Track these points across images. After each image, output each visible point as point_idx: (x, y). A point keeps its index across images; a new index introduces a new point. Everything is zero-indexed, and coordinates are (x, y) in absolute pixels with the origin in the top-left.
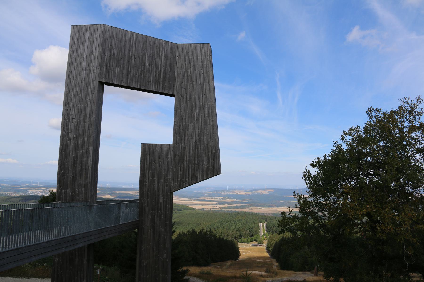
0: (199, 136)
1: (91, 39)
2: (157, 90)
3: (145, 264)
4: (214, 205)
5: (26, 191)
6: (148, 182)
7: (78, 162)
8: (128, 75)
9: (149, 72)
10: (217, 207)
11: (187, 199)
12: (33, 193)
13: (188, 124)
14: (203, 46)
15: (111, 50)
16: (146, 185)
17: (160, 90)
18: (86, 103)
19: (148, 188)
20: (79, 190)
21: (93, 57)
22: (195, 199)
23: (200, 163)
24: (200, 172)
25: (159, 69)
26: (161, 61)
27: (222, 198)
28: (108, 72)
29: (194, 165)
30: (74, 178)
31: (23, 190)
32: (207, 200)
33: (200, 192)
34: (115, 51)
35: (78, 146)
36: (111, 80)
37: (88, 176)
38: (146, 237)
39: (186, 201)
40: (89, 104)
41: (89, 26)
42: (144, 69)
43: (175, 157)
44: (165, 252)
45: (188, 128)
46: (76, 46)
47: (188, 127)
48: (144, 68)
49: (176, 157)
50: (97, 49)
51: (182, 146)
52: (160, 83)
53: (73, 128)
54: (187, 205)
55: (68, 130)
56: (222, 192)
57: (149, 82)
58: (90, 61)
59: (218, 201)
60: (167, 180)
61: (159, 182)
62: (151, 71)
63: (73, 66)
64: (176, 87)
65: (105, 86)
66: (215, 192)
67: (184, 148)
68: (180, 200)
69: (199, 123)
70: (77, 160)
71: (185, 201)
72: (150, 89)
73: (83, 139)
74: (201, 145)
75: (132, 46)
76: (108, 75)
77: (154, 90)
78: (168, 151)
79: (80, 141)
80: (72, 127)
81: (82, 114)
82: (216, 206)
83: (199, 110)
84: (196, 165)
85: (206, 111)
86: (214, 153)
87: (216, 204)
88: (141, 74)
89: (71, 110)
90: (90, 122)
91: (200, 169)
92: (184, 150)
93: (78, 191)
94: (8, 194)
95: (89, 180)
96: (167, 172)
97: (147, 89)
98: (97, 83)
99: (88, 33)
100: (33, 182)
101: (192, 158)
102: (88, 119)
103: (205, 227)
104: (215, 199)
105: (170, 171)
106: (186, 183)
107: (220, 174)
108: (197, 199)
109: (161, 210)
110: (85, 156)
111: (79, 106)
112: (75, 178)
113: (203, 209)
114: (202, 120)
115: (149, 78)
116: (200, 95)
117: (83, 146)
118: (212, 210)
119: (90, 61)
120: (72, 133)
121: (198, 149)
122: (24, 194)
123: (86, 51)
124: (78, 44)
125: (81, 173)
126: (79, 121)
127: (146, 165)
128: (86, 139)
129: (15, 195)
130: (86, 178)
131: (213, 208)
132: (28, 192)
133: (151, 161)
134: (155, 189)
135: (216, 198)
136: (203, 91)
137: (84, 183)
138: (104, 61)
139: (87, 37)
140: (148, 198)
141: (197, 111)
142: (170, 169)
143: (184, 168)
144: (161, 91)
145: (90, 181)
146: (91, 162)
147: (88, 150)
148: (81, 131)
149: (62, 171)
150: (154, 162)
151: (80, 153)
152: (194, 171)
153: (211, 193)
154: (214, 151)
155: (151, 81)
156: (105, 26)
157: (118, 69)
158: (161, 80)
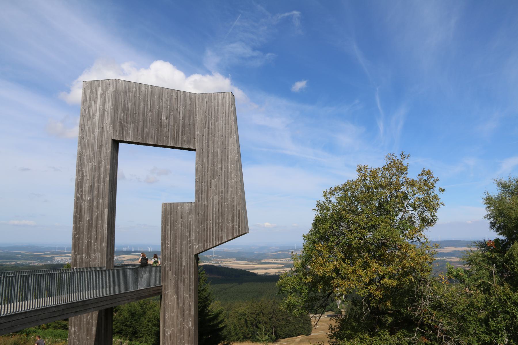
0: (222, 193)
1: (103, 96)
2: (176, 145)
3: (169, 333)
4: (280, 268)
5: (51, 259)
6: (171, 245)
7: (93, 225)
8: (143, 131)
9: (167, 126)
10: (283, 270)
11: (246, 262)
12: (59, 261)
13: (211, 181)
14: (224, 94)
15: (124, 105)
16: (168, 247)
17: (179, 145)
18: (100, 162)
19: (170, 251)
20: (94, 255)
21: (106, 113)
22: (256, 262)
23: (224, 221)
24: (224, 231)
25: (177, 122)
26: (180, 114)
27: (290, 259)
28: (122, 128)
29: (219, 225)
30: (89, 243)
31: (47, 257)
32: (271, 262)
33: (262, 253)
34: (130, 106)
35: (92, 209)
36: (125, 138)
37: (103, 240)
38: (169, 303)
39: (246, 264)
40: (103, 163)
41: (101, 82)
42: (161, 124)
43: (198, 216)
44: (190, 319)
45: (211, 185)
46: (88, 103)
47: (211, 183)
48: (161, 122)
49: (199, 217)
50: (109, 106)
51: (204, 204)
52: (179, 138)
53: (87, 189)
54: (246, 269)
55: (82, 191)
56: (289, 252)
57: (166, 137)
58: (103, 118)
59: (285, 264)
60: (190, 241)
61: (181, 245)
62: (169, 125)
63: (86, 125)
64: (197, 140)
65: (120, 144)
66: (281, 252)
67: (207, 206)
68: (238, 264)
69: (222, 178)
70: (92, 224)
71: (244, 264)
72: (168, 144)
73: (98, 201)
74: (224, 203)
75: (147, 100)
76: (122, 133)
77: (173, 146)
78: (190, 210)
79: (95, 203)
80: (86, 187)
81: (96, 175)
82: (282, 269)
83: (222, 165)
84: (220, 224)
85: (229, 165)
86: (239, 211)
87: (283, 266)
88: (158, 130)
89: (85, 170)
90: (104, 182)
91: (224, 229)
92: (207, 208)
93: (94, 256)
94: (29, 263)
95: (104, 244)
96: (190, 233)
97: (164, 145)
98: (110, 142)
99: (100, 89)
100: (59, 248)
101: (216, 217)
102: (102, 179)
103: (270, 295)
104: (281, 261)
105: (193, 232)
106: (210, 244)
107: (246, 233)
108: (259, 262)
109: (184, 273)
110: (100, 218)
111: (92, 167)
112: (91, 242)
113: (267, 273)
114: (225, 175)
115: (167, 133)
116: (222, 148)
117: (97, 209)
118: (277, 274)
119: (103, 118)
120: (87, 196)
121: (221, 206)
122: (49, 262)
123: (98, 108)
124: (90, 101)
125: (96, 237)
126: (94, 183)
127: (168, 225)
128: (101, 201)
129: (38, 264)
130: (102, 242)
131: (279, 272)
132: (54, 259)
133: (172, 222)
134: (178, 251)
135: (283, 259)
136: (225, 144)
137: (99, 247)
138: (117, 118)
139: (99, 93)
140: (170, 261)
141: (219, 166)
142: (193, 230)
143: (207, 227)
144: (180, 146)
145: (106, 245)
146: (107, 225)
147: (103, 212)
148: (95, 193)
149: (76, 235)
150: (176, 222)
151: (95, 217)
152: (219, 231)
153: (276, 253)
154: (238, 208)
155: (168, 137)
156: (117, 81)
157: (132, 125)
158: (180, 134)
